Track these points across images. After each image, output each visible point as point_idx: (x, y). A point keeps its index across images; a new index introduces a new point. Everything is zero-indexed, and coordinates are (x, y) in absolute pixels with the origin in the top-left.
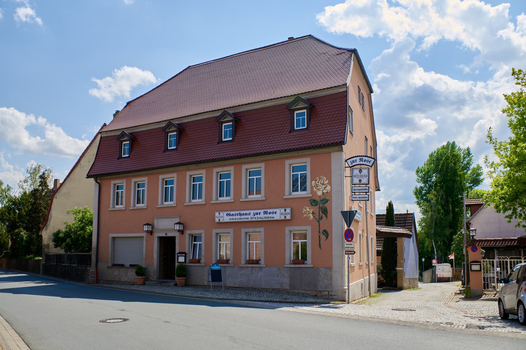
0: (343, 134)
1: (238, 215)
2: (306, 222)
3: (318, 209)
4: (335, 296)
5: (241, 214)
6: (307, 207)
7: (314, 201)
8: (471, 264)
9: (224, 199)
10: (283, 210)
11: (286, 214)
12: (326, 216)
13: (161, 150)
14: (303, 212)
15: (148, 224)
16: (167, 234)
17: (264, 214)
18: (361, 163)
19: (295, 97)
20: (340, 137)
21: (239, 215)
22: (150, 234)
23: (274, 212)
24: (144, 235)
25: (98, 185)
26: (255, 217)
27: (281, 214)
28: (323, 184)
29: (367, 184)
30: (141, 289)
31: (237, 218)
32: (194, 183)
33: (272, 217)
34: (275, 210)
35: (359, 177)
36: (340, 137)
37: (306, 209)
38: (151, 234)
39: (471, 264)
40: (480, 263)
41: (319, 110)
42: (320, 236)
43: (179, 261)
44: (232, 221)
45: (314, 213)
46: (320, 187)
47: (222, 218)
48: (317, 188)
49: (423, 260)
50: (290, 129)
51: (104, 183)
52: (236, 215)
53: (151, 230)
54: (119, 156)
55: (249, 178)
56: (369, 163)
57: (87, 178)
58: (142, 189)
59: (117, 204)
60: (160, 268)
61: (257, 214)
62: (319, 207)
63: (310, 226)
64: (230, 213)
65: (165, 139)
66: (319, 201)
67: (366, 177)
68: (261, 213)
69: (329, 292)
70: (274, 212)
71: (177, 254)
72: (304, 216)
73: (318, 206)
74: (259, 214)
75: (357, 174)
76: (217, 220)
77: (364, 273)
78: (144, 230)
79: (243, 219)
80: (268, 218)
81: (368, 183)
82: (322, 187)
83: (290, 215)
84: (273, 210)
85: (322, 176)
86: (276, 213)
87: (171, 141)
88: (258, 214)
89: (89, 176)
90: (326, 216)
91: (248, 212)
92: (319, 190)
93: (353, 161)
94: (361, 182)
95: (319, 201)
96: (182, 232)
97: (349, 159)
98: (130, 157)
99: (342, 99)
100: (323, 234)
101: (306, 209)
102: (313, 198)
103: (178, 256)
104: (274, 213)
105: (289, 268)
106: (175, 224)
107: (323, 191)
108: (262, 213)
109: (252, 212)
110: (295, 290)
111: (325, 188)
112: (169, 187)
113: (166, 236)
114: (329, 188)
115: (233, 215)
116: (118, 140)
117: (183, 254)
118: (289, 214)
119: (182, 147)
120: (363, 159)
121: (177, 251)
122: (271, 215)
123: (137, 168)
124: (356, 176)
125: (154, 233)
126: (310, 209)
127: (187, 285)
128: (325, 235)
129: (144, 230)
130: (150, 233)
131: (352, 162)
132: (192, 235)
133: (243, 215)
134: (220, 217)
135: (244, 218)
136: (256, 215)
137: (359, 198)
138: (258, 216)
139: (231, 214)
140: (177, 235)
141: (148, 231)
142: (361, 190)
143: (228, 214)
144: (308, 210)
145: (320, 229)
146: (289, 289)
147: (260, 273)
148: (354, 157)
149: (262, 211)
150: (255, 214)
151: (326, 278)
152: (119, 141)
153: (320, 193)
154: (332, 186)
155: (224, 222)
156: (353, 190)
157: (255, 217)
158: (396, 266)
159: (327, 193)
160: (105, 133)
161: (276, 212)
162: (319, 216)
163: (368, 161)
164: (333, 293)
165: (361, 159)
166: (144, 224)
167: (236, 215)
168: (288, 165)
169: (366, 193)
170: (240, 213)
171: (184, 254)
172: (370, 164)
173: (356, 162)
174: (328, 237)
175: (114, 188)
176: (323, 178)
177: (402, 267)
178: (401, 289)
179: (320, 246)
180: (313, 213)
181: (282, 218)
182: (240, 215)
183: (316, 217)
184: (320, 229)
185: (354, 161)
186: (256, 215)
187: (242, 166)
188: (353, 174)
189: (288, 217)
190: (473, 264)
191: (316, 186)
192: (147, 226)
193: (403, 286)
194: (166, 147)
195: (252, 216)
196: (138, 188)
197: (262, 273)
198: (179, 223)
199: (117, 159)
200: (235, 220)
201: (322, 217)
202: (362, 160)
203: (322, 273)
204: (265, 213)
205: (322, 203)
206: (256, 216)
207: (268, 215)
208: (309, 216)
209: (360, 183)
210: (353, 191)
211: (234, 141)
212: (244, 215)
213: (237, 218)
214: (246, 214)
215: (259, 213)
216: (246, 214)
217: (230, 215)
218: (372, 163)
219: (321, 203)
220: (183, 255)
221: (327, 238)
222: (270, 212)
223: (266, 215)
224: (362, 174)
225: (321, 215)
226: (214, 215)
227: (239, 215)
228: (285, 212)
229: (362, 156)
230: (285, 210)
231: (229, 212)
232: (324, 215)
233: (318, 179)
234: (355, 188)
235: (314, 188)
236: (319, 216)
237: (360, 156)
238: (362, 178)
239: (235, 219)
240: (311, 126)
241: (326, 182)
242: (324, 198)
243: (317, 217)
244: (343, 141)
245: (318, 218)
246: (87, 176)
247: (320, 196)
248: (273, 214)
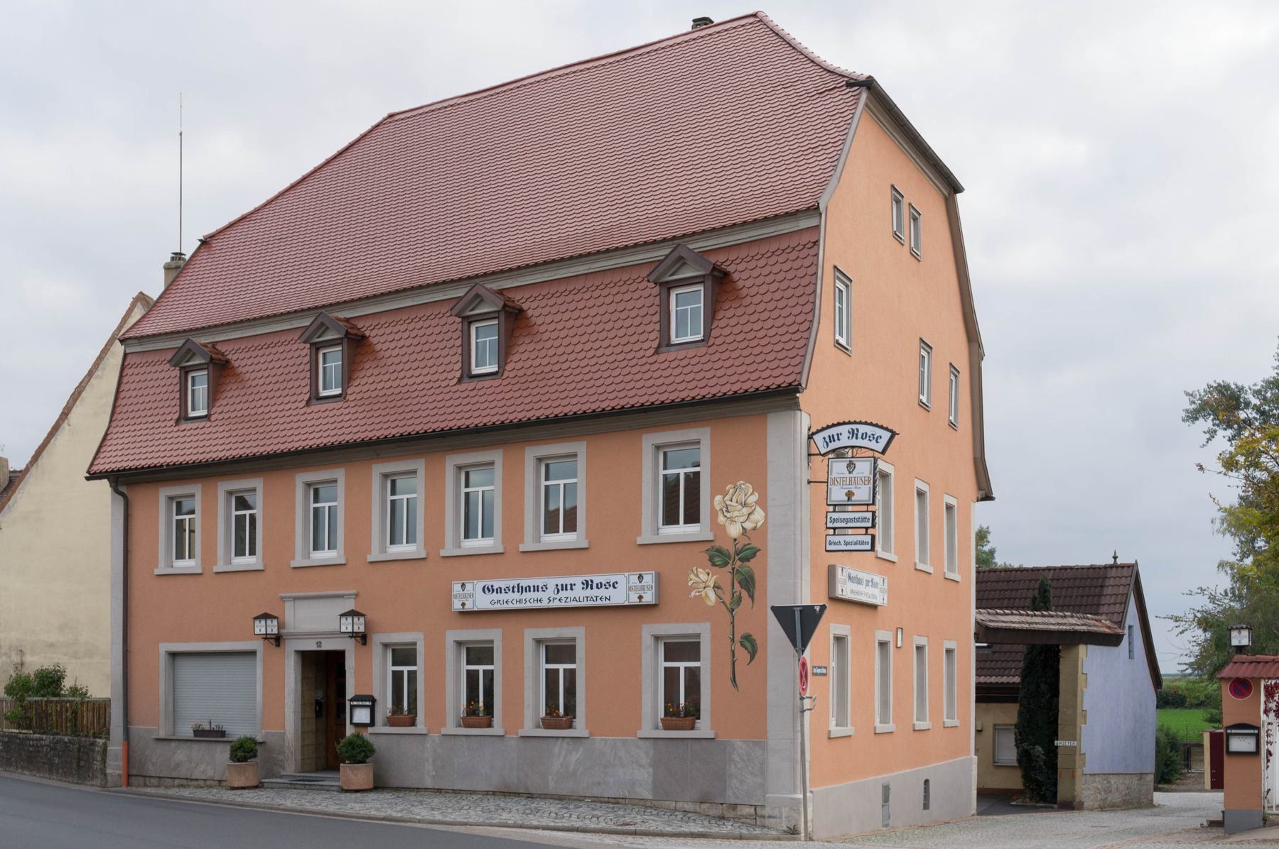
0: (798, 359)
1: (513, 592)
2: (699, 610)
3: (730, 576)
4: (771, 819)
5: (522, 587)
6: (699, 570)
7: (719, 551)
8: (1229, 731)
9: (478, 544)
10: (634, 579)
11: (642, 588)
12: (752, 597)
13: (169, 417)
14: (690, 584)
15: (266, 616)
16: (320, 643)
17: (583, 588)
18: (854, 442)
19: (674, 244)
20: (790, 370)
21: (516, 589)
22: (274, 643)
23: (611, 584)
24: (257, 645)
25: (120, 498)
26: (558, 597)
27: (630, 589)
28: (745, 505)
29: (868, 505)
30: (247, 800)
31: (512, 600)
32: (548, 483)
33: (606, 598)
34: (613, 579)
35: (848, 483)
36: (790, 370)
37: (697, 576)
38: (364, 643)
39: (1229, 731)
40: (1256, 731)
41: (740, 284)
42: (733, 652)
43: (356, 720)
44: (497, 607)
45: (718, 588)
46: (736, 513)
47: (471, 600)
48: (728, 515)
50: (658, 340)
51: (140, 497)
52: (509, 590)
53: (275, 631)
54: (178, 413)
55: (544, 483)
56: (877, 442)
57: (88, 479)
58: (327, 505)
59: (180, 555)
60: (303, 740)
61: (564, 587)
62: (733, 569)
63: (708, 625)
64: (492, 586)
65: (178, 385)
66: (732, 552)
67: (866, 482)
68: (575, 585)
69: (758, 809)
70: (611, 584)
71: (351, 700)
72: (693, 594)
73: (729, 568)
74: (572, 589)
75: (841, 476)
76: (457, 606)
78: (257, 631)
79: (510, 603)
80: (595, 599)
81: (871, 502)
82: (739, 513)
83: (653, 591)
84: (543, 580)
85: (741, 482)
86: (616, 586)
87: (480, 345)
88: (569, 587)
89: (95, 473)
90: (750, 596)
91: (539, 582)
92: (732, 520)
93: (832, 439)
94: (853, 498)
95: (732, 552)
96: (363, 638)
97: (818, 431)
98: (213, 418)
99: (805, 252)
100: (742, 645)
101: (697, 576)
102: (717, 544)
103: (352, 707)
104: (610, 586)
105: (651, 740)
106: (342, 615)
107: (743, 525)
108: (579, 586)
109: (552, 582)
110: (667, 802)
111: (749, 514)
112: (245, 515)
113: (319, 649)
114: (759, 515)
115: (499, 590)
116: (175, 366)
117: (365, 701)
118: (650, 588)
119: (359, 388)
120: (858, 430)
121: (350, 692)
122: (602, 592)
123: (300, 443)
124: (838, 480)
125: (284, 639)
126: (708, 574)
127: (379, 786)
128: (746, 648)
129: (257, 631)
130: (273, 641)
131: (828, 440)
133: (526, 591)
134: (465, 596)
135: (529, 600)
136: (562, 590)
137: (847, 543)
138: (569, 593)
139: (495, 588)
140: (348, 646)
141: (268, 636)
142: (850, 520)
143: (488, 588)
144: (703, 577)
145: (733, 633)
146: (651, 798)
147: (574, 753)
148: (834, 425)
149: (578, 580)
150: (560, 588)
151: (750, 768)
152: (178, 368)
153: (734, 531)
154: (770, 510)
155: (476, 609)
156: (828, 522)
157: (558, 597)
158: (1055, 735)
159: (754, 529)
160: (137, 341)
161: (617, 583)
162: (733, 594)
163: (874, 438)
164: (767, 811)
165: (853, 430)
166: (255, 616)
167: (509, 590)
168: (532, 460)
169: (867, 528)
170: (518, 585)
171: (370, 702)
172: (880, 447)
173: (839, 439)
174: (754, 656)
175: (306, 497)
176: (743, 486)
177: (1073, 737)
178: (1070, 805)
179: (734, 680)
180: (716, 587)
181: (630, 601)
182: (518, 591)
183: (723, 596)
184: (733, 633)
185: (833, 436)
186: (562, 590)
188: (831, 474)
189: (649, 598)
190: (1233, 731)
191: (724, 509)
192: (350, 619)
193: (1074, 797)
194: (313, 391)
195: (550, 592)
196: (314, 502)
197: (579, 755)
198: (353, 614)
199: (173, 422)
200: (601, 602)
201: (740, 598)
202: (857, 435)
203: (738, 753)
204: (588, 585)
205: (739, 559)
206: (563, 594)
207: (595, 592)
208: (706, 594)
209: (849, 500)
210: (830, 525)
211: (502, 375)
212: (530, 591)
213: (510, 601)
214: (536, 589)
215: (571, 585)
216: (536, 589)
217: (490, 590)
218: (883, 442)
219: (737, 558)
220: (368, 703)
221: (752, 658)
222: (601, 583)
223: (589, 592)
224: (855, 474)
225: (738, 593)
226: (450, 590)
227: (516, 589)
228: (640, 582)
229: (855, 423)
230: (640, 577)
231: (489, 583)
232: (744, 594)
233: (731, 491)
234: (835, 516)
235: (720, 513)
236: (733, 594)
237: (849, 423)
238: (856, 488)
239: (506, 602)
240: (714, 333)
241: (755, 498)
242: (745, 546)
243: (728, 600)
244: (796, 383)
245: (728, 601)
246: (88, 475)
247: (735, 540)
248: (607, 588)
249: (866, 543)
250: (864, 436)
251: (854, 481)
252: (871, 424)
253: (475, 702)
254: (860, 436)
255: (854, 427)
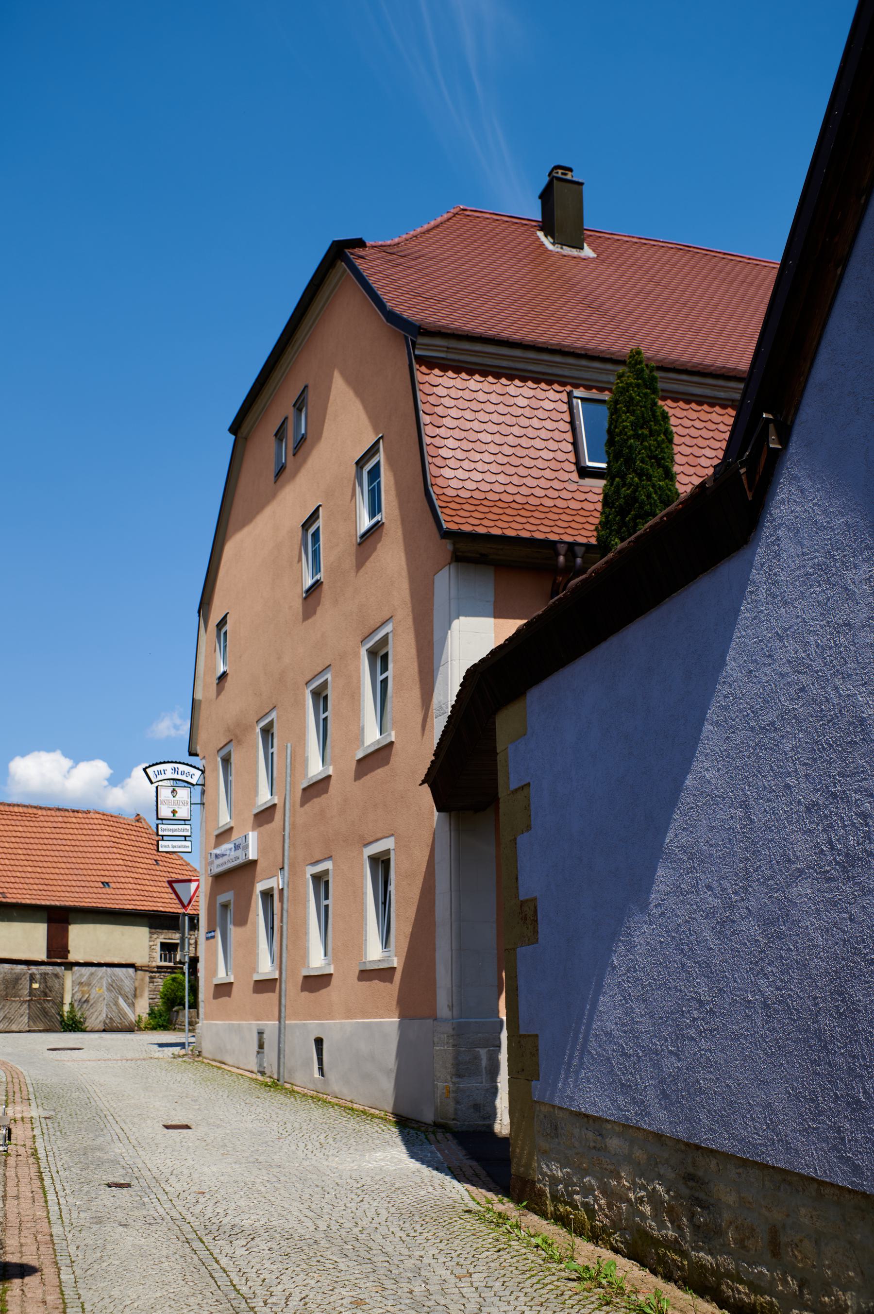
49: (196, 921)
77: (284, 960)
88: (163, 772)
93: (160, 773)
94: (176, 815)
131: (157, 773)
132: (383, 862)
187: (66, 931)
224: (177, 798)
249: (187, 847)
250: (183, 773)
251: (177, 803)
252: (187, 764)
253: (706, 483)
254: (180, 773)
255: (176, 765)
